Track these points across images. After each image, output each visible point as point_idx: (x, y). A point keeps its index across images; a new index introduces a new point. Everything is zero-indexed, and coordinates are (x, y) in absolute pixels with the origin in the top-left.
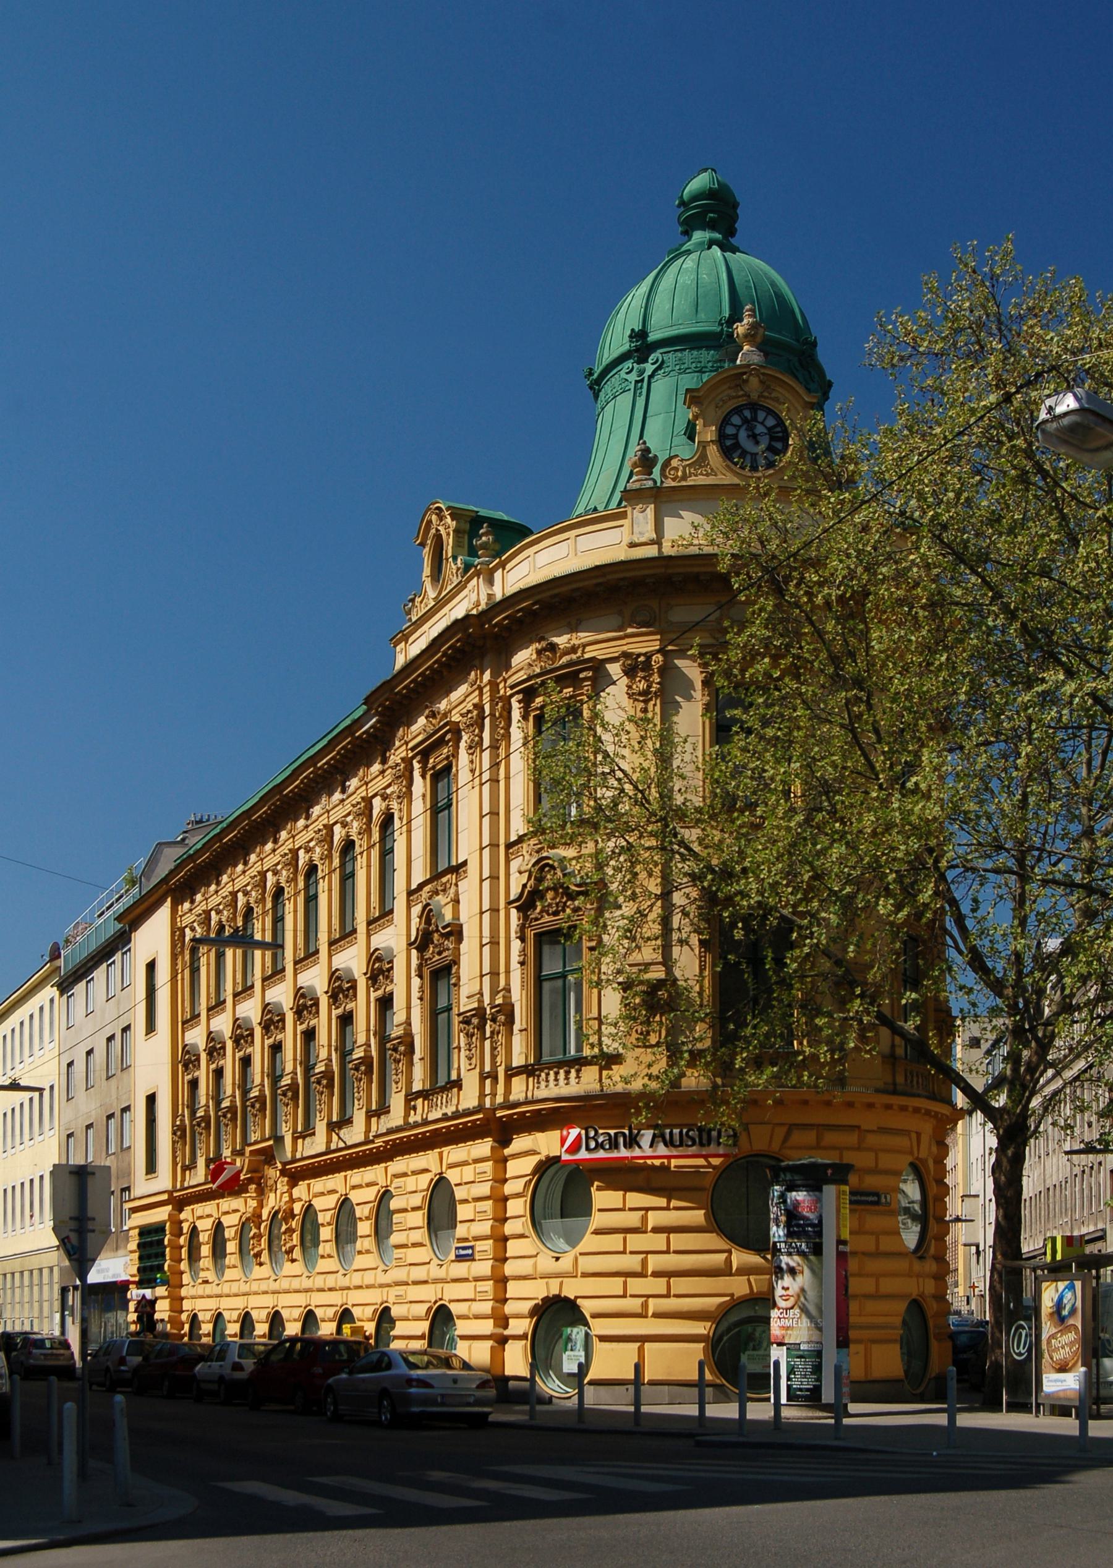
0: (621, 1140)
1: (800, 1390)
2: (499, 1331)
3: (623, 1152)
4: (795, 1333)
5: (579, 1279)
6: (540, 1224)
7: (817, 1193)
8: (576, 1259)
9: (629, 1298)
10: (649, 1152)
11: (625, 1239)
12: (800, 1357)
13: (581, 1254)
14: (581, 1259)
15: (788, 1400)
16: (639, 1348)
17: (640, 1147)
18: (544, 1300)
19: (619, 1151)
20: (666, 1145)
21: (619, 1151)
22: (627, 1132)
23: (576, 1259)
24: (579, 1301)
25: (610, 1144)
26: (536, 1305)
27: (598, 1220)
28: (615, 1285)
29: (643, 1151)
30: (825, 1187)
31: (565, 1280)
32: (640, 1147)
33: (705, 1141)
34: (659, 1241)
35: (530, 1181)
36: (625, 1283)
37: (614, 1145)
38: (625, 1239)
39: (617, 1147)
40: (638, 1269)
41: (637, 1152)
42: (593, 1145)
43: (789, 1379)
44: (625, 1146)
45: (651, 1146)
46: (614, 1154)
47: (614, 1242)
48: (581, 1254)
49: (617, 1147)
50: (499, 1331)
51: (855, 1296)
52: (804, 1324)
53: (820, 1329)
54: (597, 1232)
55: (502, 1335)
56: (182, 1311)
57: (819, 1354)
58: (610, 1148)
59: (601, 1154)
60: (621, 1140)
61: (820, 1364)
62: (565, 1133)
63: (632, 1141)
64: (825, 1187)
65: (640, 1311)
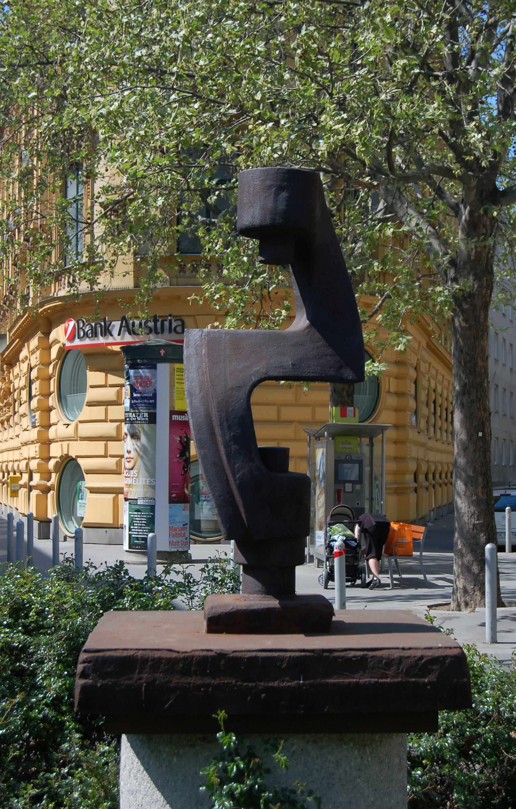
0: (99, 330)
1: (137, 539)
2: (44, 482)
3: (101, 340)
4: (133, 490)
5: (79, 442)
6: (65, 398)
7: (153, 370)
8: (77, 426)
9: (109, 458)
10: (118, 339)
11: (106, 410)
12: (138, 511)
13: (81, 422)
14: (81, 426)
15: (130, 548)
16: (114, 498)
17: (111, 335)
18: (61, 457)
19: (98, 339)
20: (130, 334)
21: (98, 339)
22: (103, 323)
23: (77, 426)
24: (80, 461)
25: (92, 333)
26: (57, 462)
27: (91, 394)
28: (98, 447)
29: (114, 339)
30: (159, 365)
31: (71, 442)
32: (111, 335)
33: (159, 330)
34: (287, 414)
35: (57, 363)
36: (106, 446)
37: (95, 334)
38: (106, 410)
39: (96, 336)
40: (114, 434)
41: (110, 340)
42: (82, 334)
43: (130, 530)
44: (102, 335)
45: (119, 335)
46: (96, 342)
47: (98, 412)
48: (81, 422)
49: (96, 336)
50: (44, 482)
51: (293, 457)
52: (141, 483)
53: (153, 487)
54: (91, 404)
55: (46, 485)
56: (50, 458)
57: (152, 508)
58: (92, 337)
59: (87, 341)
60: (99, 330)
61: (153, 517)
62: (67, 325)
63: (107, 331)
64: (159, 365)
65: (115, 468)
